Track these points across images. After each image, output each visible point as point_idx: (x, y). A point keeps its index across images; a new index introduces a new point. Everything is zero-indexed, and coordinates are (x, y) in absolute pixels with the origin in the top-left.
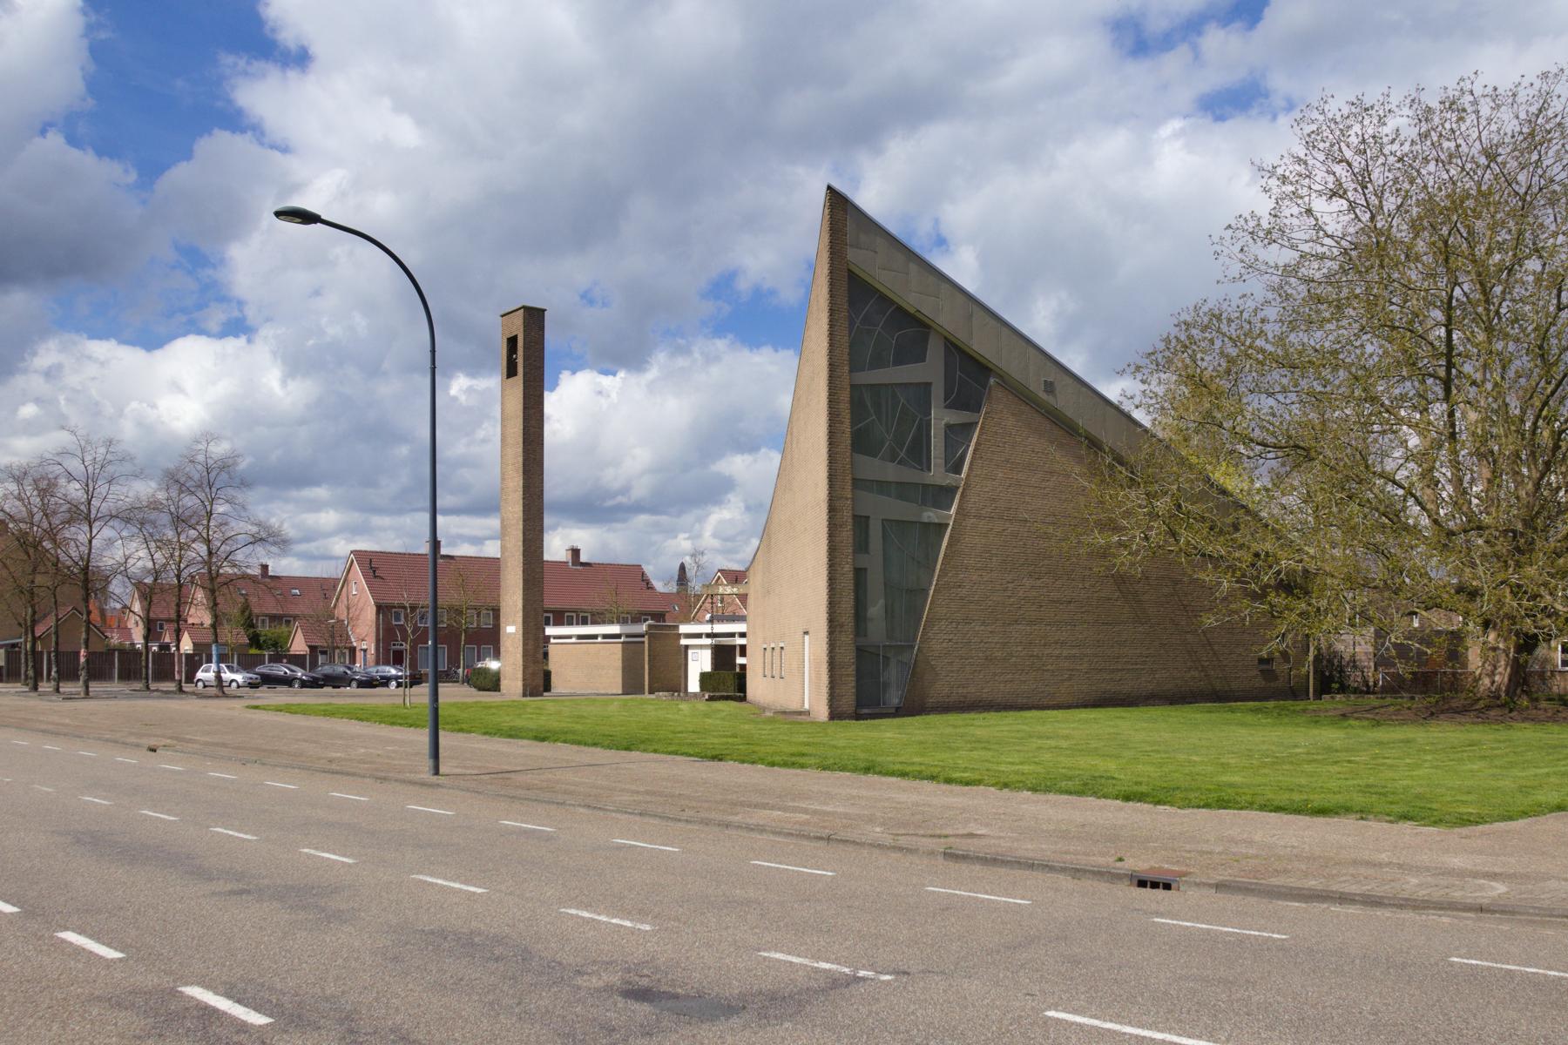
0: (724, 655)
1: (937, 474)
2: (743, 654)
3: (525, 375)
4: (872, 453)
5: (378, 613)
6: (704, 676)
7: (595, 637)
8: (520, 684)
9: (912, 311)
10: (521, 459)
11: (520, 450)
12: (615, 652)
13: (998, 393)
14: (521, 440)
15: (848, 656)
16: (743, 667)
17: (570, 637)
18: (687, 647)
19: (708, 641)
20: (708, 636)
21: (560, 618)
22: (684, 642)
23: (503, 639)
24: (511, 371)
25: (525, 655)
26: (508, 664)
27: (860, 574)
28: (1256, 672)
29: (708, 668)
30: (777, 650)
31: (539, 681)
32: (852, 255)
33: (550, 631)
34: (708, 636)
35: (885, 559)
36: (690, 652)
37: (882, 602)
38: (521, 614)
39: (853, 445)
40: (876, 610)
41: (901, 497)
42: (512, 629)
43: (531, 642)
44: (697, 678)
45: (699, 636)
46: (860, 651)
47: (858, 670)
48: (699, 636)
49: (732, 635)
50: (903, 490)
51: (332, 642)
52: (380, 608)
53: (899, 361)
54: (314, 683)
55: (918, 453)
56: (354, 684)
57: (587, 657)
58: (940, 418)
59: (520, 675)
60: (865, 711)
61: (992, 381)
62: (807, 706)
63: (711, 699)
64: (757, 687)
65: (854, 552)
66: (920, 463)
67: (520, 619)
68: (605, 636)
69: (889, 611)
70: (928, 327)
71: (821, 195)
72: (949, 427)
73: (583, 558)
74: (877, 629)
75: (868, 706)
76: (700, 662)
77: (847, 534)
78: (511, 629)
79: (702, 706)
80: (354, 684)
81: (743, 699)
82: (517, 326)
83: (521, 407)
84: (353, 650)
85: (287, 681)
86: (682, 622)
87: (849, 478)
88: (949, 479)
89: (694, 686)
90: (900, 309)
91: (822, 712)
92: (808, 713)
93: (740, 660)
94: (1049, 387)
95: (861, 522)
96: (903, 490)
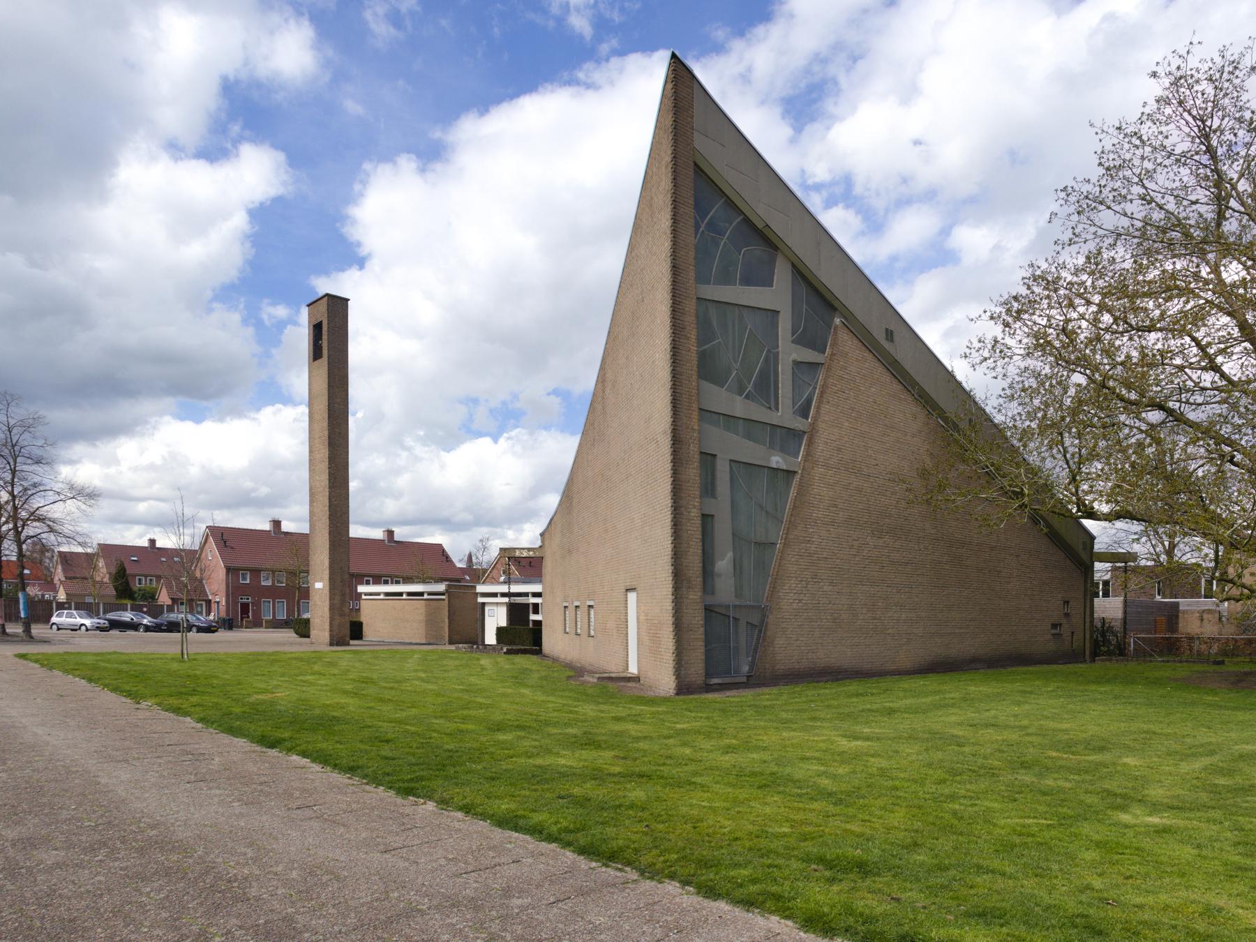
0: (518, 612)
1: (784, 415)
2: (536, 611)
3: (329, 357)
4: (719, 381)
5: (227, 574)
6: (500, 630)
7: (401, 594)
8: (327, 634)
9: (760, 225)
10: (326, 433)
11: (325, 424)
13: (844, 336)
14: (326, 416)
15: (696, 618)
16: (538, 623)
17: (378, 594)
18: (484, 604)
19: (506, 600)
20: (503, 595)
21: (362, 578)
22: (481, 600)
23: (312, 593)
25: (332, 608)
26: (319, 611)
28: (1050, 637)
29: (503, 623)
30: (584, 609)
32: (699, 142)
33: (361, 589)
34: (503, 595)
35: (732, 507)
36: (487, 608)
37: (730, 554)
38: (327, 572)
39: (699, 372)
40: (723, 564)
41: (749, 436)
43: (338, 598)
44: (494, 632)
45: (494, 595)
46: (709, 610)
47: (706, 633)
48: (494, 595)
49: (526, 595)
50: (751, 428)
51: (195, 597)
52: (229, 570)
53: (747, 281)
54: (157, 628)
55: (765, 389)
56: (194, 629)
58: (789, 353)
59: (327, 627)
60: (716, 681)
61: (837, 321)
62: (633, 669)
63: (509, 652)
64: (553, 641)
65: (701, 497)
66: (769, 402)
67: (326, 575)
68: (409, 594)
69: (737, 565)
70: (776, 248)
72: (796, 364)
73: (396, 538)
74: (725, 590)
75: (718, 675)
76: (496, 618)
77: (692, 473)
78: (319, 585)
79: (503, 661)
80: (194, 629)
81: (539, 652)
83: (325, 385)
84: (209, 602)
85: (134, 626)
87: (695, 406)
88: (799, 424)
89: (491, 638)
90: (747, 221)
91: (665, 681)
92: (636, 679)
93: (533, 617)
94: (889, 335)
96: (751, 428)
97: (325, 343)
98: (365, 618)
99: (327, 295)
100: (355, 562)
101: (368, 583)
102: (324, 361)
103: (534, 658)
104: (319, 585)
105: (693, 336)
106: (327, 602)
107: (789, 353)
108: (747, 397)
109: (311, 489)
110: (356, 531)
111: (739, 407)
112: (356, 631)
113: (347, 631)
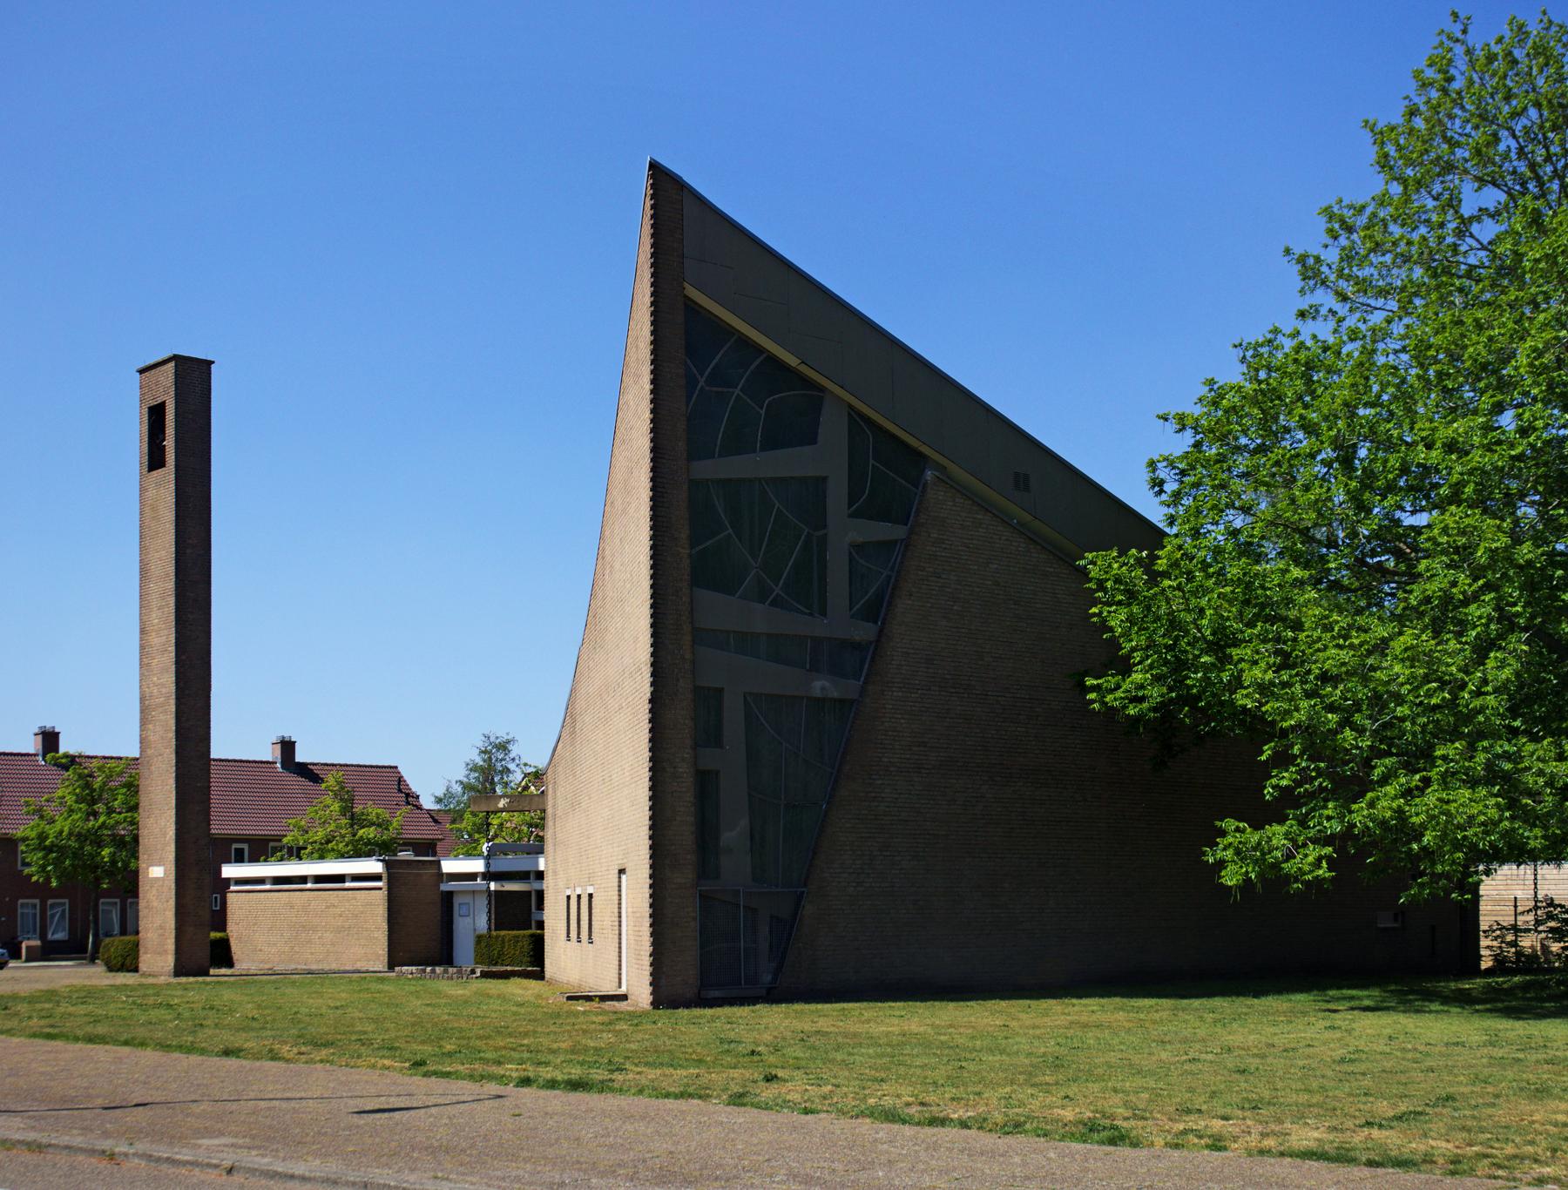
12: (376, 901)
14: (171, 569)
22: (444, 887)
23: (143, 888)
24: (155, 460)
27: (706, 783)
31: (205, 947)
33: (229, 871)
36: (457, 901)
37: (744, 823)
38: (172, 847)
40: (734, 835)
42: (158, 872)
57: (309, 918)
58: (846, 531)
61: (929, 475)
63: (485, 975)
71: (641, 182)
72: (858, 548)
78: (156, 872)
81: (540, 976)
82: (165, 387)
86: (447, 856)
91: (638, 985)
95: (709, 701)
97: (170, 443)
98: (235, 930)
99: (175, 358)
100: (226, 814)
101: (239, 859)
102: (168, 473)
103: (532, 983)
104: (156, 872)
105: (684, 534)
106: (172, 902)
107: (846, 531)
108: (774, 604)
109: (142, 699)
110: (220, 748)
111: (761, 619)
112: (222, 955)
113: (204, 954)
